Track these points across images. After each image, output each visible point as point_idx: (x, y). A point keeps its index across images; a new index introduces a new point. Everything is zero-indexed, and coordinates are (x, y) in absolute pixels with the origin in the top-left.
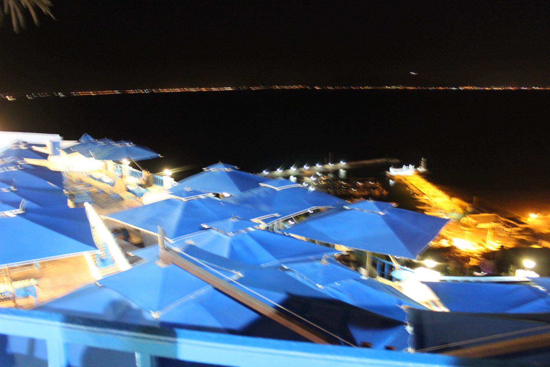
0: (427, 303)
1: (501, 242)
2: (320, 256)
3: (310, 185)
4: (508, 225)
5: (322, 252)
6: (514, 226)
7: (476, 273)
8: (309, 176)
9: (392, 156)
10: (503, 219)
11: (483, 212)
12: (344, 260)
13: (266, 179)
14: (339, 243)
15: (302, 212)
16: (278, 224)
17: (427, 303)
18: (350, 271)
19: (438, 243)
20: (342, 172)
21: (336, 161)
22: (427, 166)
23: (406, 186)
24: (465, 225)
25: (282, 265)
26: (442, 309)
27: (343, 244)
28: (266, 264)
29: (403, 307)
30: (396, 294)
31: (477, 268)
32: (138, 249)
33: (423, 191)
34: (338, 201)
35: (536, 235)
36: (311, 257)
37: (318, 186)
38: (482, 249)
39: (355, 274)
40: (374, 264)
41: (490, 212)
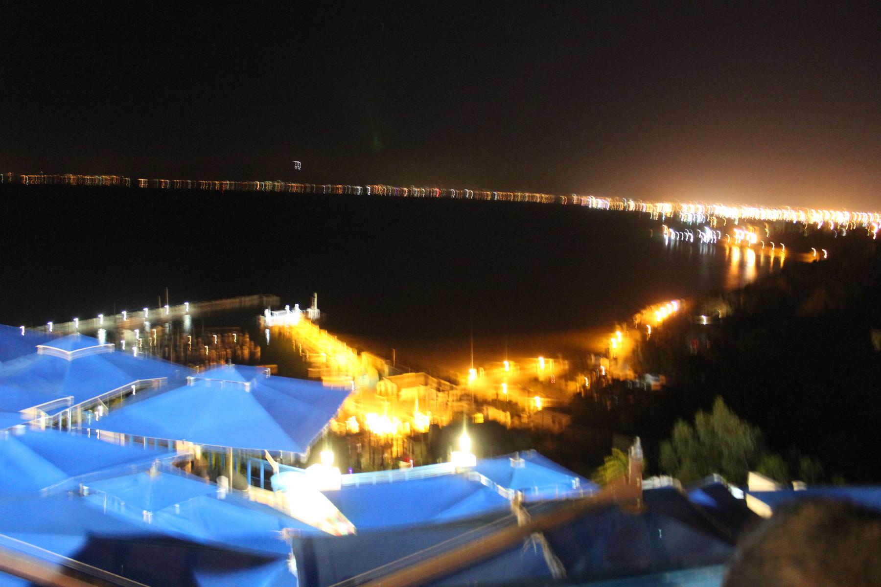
3: (129, 344)
5: (149, 457)
8: (132, 329)
9: (268, 292)
12: (181, 464)
13: (48, 339)
14: (181, 439)
15: (121, 389)
16: (74, 413)
18: (205, 484)
20: (187, 322)
21: (176, 302)
23: (289, 340)
27: (188, 440)
28: (53, 487)
32: (539, 464)
34: (177, 370)
35: (479, 403)
36: (133, 466)
37: (145, 346)
38: (408, 431)
40: (244, 468)
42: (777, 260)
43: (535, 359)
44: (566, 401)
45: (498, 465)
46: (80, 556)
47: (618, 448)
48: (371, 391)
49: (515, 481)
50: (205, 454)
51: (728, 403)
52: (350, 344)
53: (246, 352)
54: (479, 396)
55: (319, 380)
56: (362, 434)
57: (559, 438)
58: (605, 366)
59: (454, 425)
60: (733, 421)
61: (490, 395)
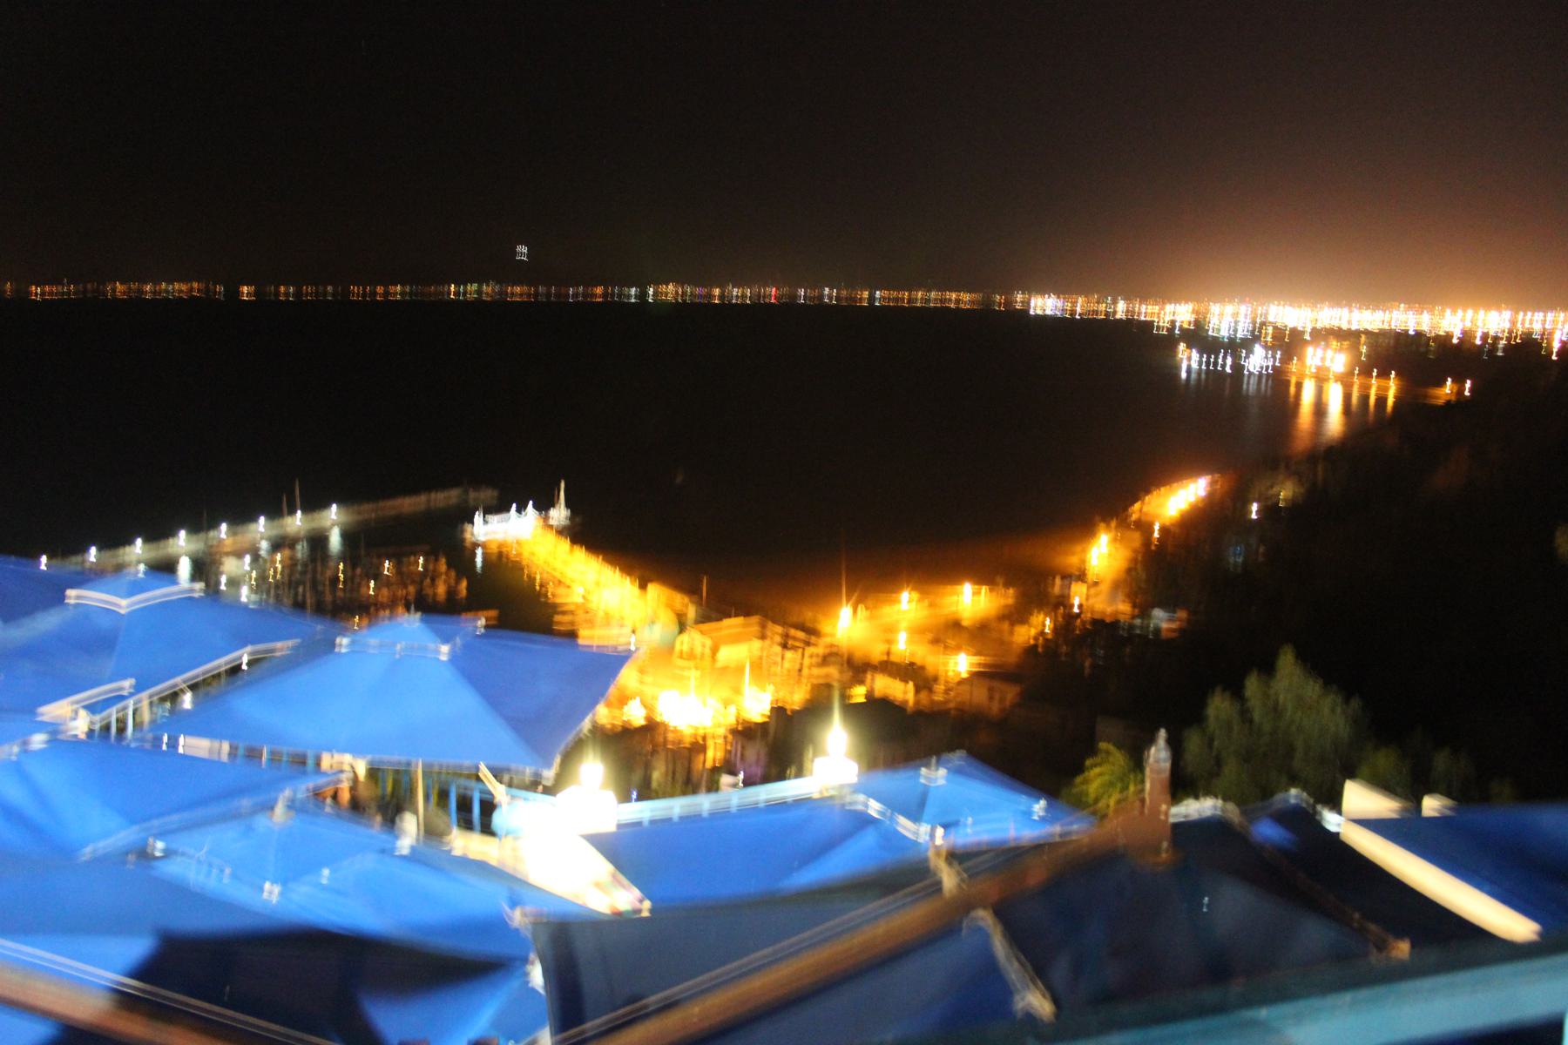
1: (771, 688)
2: (574, 732)
3: (234, 583)
5: (276, 784)
8: (239, 555)
9: (477, 483)
10: (779, 629)
11: (729, 616)
13: (85, 578)
14: (329, 750)
20: (335, 541)
21: (314, 504)
22: (568, 505)
23: (517, 567)
29: (518, 918)
31: (729, 767)
34: (319, 627)
35: (858, 668)
36: (246, 803)
38: (730, 720)
40: (443, 795)
42: (1381, 401)
43: (959, 587)
44: (1012, 659)
45: (897, 781)
46: (144, 972)
47: (1109, 742)
48: (665, 653)
49: (930, 810)
50: (373, 773)
51: (1302, 657)
52: (627, 569)
53: (441, 589)
54: (858, 655)
55: (572, 635)
56: (651, 728)
57: (1001, 724)
58: (1078, 596)
59: (816, 709)
60: (1312, 689)
61: (877, 652)
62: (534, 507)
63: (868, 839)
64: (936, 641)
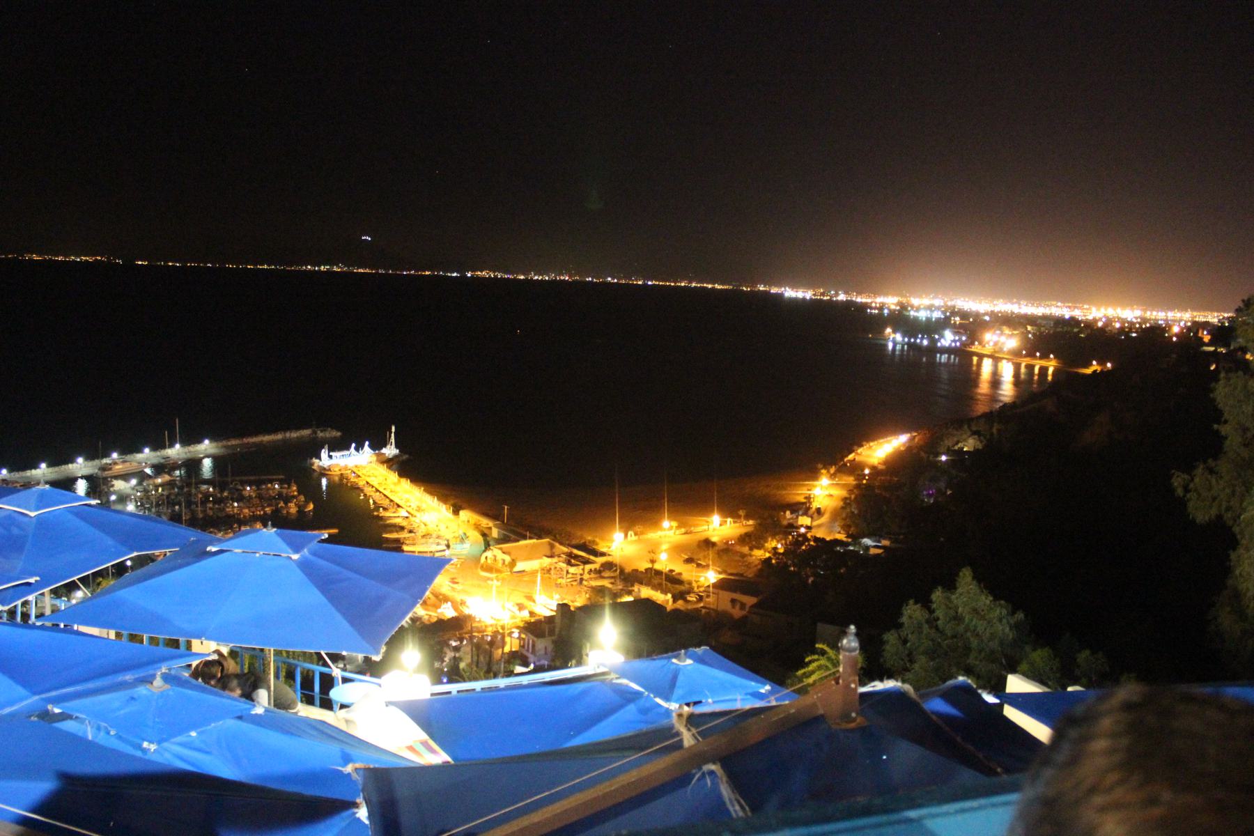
0: (411, 748)
3: (123, 499)
4: (571, 559)
6: (587, 562)
7: (519, 669)
8: (125, 477)
9: (324, 424)
11: (525, 538)
12: (210, 673)
14: (198, 637)
17: (411, 748)
18: (232, 699)
19: (436, 612)
21: (191, 438)
22: (397, 447)
23: (358, 489)
24: (489, 569)
25: (50, 707)
26: (440, 757)
30: (338, 739)
31: (519, 657)
33: (397, 500)
34: (193, 535)
35: (630, 578)
36: (128, 677)
37: (143, 503)
39: (243, 705)
40: (290, 676)
41: (540, 537)
45: (655, 666)
46: (46, 806)
49: (678, 692)
51: (978, 578)
52: (443, 498)
53: (293, 509)
55: (397, 546)
56: (457, 625)
57: (739, 625)
59: (590, 611)
60: (985, 600)
61: (643, 566)
62: (369, 446)
63: (630, 710)
64: (689, 561)
